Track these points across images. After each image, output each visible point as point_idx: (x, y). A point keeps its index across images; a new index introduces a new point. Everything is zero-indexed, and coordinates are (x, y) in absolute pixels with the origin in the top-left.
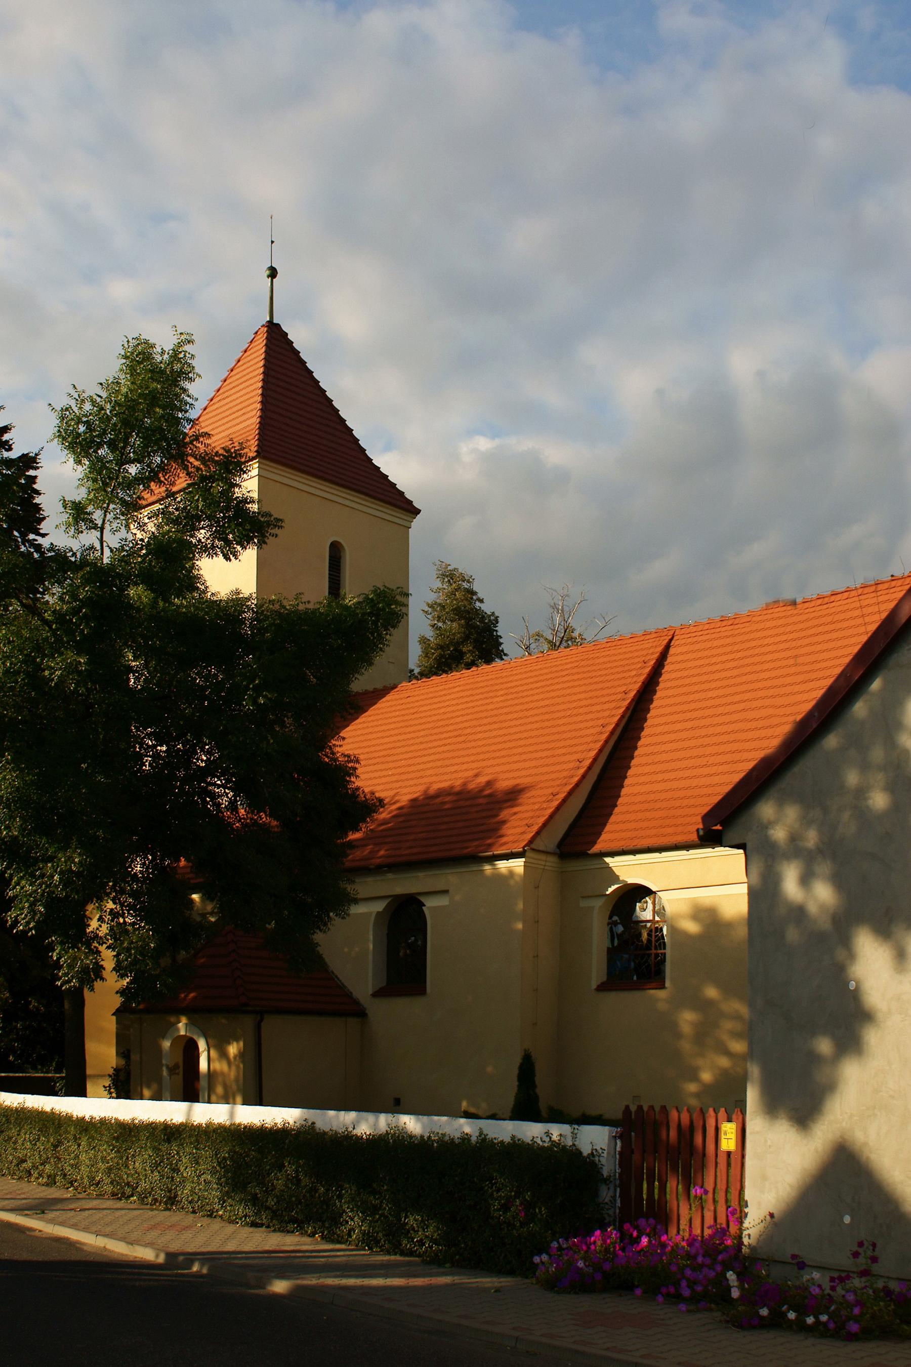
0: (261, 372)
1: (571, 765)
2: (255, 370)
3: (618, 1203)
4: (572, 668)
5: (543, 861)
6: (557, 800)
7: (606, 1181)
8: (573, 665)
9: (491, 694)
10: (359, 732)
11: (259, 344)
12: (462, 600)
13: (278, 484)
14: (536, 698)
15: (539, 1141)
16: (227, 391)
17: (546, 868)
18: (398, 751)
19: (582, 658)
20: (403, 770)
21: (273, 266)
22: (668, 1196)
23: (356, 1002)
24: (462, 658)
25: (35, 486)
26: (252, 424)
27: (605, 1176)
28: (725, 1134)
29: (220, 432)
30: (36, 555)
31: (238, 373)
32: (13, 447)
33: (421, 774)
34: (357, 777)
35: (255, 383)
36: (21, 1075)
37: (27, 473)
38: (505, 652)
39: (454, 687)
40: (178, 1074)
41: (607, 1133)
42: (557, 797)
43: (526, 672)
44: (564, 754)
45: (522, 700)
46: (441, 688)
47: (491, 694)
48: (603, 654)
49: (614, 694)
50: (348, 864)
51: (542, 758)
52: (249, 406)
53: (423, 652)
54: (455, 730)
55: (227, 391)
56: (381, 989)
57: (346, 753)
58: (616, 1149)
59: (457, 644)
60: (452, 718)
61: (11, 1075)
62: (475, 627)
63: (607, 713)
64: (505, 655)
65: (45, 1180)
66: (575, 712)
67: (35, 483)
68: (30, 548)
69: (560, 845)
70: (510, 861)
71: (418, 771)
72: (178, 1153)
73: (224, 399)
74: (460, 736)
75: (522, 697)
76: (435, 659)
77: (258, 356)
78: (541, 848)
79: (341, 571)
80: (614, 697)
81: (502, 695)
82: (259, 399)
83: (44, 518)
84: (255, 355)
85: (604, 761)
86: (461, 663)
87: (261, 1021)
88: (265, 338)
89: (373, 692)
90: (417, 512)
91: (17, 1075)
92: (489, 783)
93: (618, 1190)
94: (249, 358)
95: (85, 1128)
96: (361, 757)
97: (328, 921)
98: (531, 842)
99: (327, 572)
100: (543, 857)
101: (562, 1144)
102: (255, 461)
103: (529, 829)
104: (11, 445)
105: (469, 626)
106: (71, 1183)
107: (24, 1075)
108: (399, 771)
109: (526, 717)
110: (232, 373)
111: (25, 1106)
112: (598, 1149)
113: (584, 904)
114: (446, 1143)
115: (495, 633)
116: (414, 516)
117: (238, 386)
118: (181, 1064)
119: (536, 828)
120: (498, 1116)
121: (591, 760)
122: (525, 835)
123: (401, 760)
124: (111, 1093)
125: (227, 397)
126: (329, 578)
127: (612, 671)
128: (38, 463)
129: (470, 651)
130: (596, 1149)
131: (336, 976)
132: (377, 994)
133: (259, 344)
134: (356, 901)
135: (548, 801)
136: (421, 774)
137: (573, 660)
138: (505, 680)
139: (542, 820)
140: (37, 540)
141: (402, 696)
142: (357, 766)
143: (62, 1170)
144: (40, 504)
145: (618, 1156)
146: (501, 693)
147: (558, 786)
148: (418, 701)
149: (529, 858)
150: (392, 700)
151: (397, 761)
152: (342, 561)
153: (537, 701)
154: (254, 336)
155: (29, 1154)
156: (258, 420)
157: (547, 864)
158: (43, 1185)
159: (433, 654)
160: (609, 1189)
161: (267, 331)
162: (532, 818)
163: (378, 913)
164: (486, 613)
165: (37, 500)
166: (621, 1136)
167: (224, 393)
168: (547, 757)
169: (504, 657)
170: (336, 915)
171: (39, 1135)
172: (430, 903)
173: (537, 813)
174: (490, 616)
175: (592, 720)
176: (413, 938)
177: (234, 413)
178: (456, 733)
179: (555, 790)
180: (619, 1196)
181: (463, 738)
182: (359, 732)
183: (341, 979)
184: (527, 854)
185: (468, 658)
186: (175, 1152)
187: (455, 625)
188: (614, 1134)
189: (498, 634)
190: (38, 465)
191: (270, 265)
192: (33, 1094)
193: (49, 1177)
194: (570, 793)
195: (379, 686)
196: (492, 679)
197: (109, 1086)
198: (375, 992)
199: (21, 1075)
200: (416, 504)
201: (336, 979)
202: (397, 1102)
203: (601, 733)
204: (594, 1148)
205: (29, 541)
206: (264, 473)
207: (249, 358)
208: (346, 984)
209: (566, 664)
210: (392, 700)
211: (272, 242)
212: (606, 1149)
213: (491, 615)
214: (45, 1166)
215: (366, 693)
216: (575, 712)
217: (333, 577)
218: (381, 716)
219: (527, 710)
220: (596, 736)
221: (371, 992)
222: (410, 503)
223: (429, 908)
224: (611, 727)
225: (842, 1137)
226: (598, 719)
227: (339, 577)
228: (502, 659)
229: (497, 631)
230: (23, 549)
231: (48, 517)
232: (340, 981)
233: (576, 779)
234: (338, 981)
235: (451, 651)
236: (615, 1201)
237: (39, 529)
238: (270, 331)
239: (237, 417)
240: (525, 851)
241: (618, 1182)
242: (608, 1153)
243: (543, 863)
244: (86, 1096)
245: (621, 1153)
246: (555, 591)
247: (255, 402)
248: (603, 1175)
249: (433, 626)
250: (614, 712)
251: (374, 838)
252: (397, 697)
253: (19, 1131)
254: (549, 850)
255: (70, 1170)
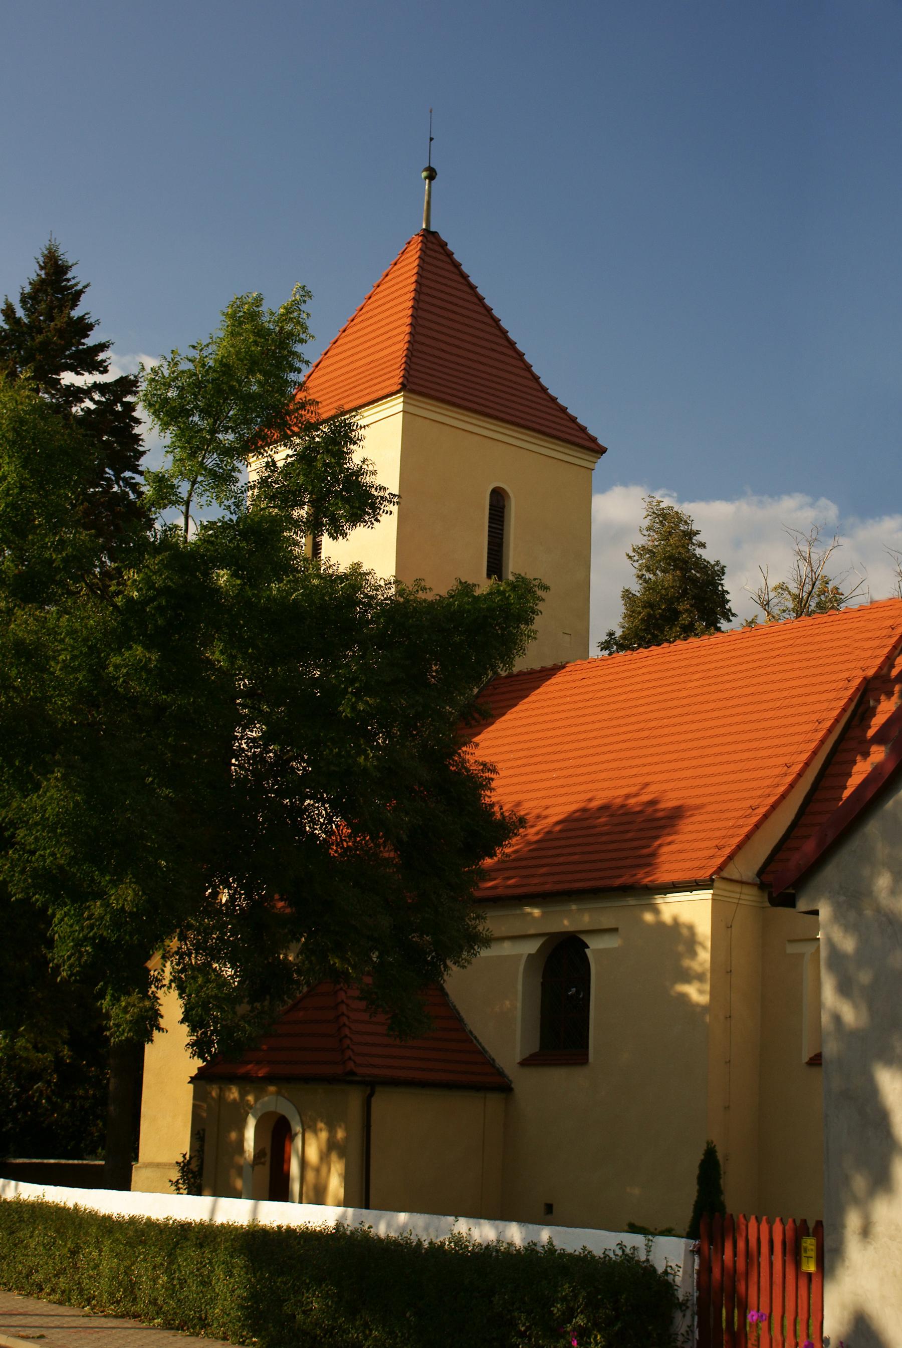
0: (412, 289)
1: (777, 771)
2: (405, 286)
3: (697, 1336)
4: (786, 647)
5: (737, 893)
6: (756, 815)
7: (683, 1306)
8: (786, 643)
9: (683, 678)
10: (519, 723)
11: (412, 256)
12: (678, 547)
13: (428, 421)
14: (740, 683)
15: (612, 1255)
16: (371, 310)
17: (741, 902)
18: (566, 747)
19: (797, 634)
20: (571, 772)
21: (432, 166)
22: (748, 1329)
23: (500, 1073)
24: (677, 619)
25: (134, 414)
26: (398, 350)
27: (680, 1301)
28: (806, 1251)
29: (360, 359)
30: (132, 496)
31: (385, 289)
32: (108, 368)
33: (593, 777)
34: (491, 790)
35: (404, 302)
36: (76, 1162)
37: (124, 400)
38: (733, 612)
39: (640, 668)
40: (264, 1164)
41: (683, 1247)
42: (757, 811)
43: (728, 651)
44: (770, 757)
45: (721, 687)
46: (624, 668)
47: (683, 678)
48: (824, 630)
49: (834, 681)
50: (477, 894)
51: (741, 761)
52: (395, 328)
53: (627, 610)
54: (638, 722)
55: (371, 310)
56: (531, 1056)
57: (481, 760)
58: (693, 1267)
59: (670, 601)
60: (635, 706)
61: (63, 1161)
62: (694, 580)
63: (825, 705)
64: (733, 615)
65: (58, 1296)
66: (786, 702)
67: (134, 410)
68: (126, 487)
69: (761, 873)
70: (694, 893)
71: (589, 773)
72: (210, 1263)
73: (367, 319)
74: (643, 730)
75: (722, 683)
76: (641, 619)
77: (410, 270)
78: (736, 876)
79: (505, 523)
80: (834, 686)
81: (697, 680)
82: (409, 321)
83: (144, 452)
84: (407, 268)
85: (820, 766)
86: (676, 626)
87: (371, 1095)
88: (418, 249)
89: (540, 671)
90: (603, 451)
91: (71, 1162)
92: (653, 802)
93: (696, 1318)
94: (398, 273)
95: (108, 1228)
96: (499, 766)
97: (445, 970)
98: (721, 868)
99: (487, 524)
100: (737, 888)
101: (636, 1258)
102: (399, 395)
103: (720, 853)
104: (107, 366)
105: (686, 580)
106: (88, 1300)
107: (80, 1162)
108: (565, 773)
109: (726, 708)
110: (379, 289)
111: (44, 1200)
112: (674, 1266)
113: (791, 949)
114: (512, 1255)
115: (720, 588)
116: (599, 456)
117: (384, 304)
118: (268, 1151)
119: (727, 851)
120: (674, 1232)
121: (802, 765)
122: (714, 860)
123: (569, 759)
124: (178, 1189)
125: (371, 317)
126: (489, 531)
127: (833, 652)
128: (138, 387)
129: (686, 610)
130: (671, 1267)
131: (475, 1038)
132: (526, 1063)
133: (412, 256)
134: (487, 942)
135: (745, 817)
136: (593, 777)
137: (786, 637)
138: (702, 660)
139: (736, 841)
140: (134, 478)
141: (574, 677)
142: (492, 776)
143: (79, 1283)
144: (140, 435)
145: (695, 1276)
146: (697, 676)
147: (760, 797)
148: (594, 684)
149: (719, 889)
150: (562, 683)
151: (564, 760)
152: (506, 510)
153: (741, 687)
154: (406, 246)
155: (41, 1262)
156: (406, 346)
157: (743, 897)
158: (55, 1303)
159: (640, 613)
160: (684, 1316)
161: (421, 241)
162: (724, 837)
163: (530, 955)
164: (708, 562)
165: (137, 430)
166: (698, 1251)
167: (367, 312)
168: (748, 759)
169: (731, 618)
170: (455, 963)
171: (54, 1238)
172: (595, 945)
173: (731, 832)
174: (713, 566)
175: (806, 713)
176: (574, 990)
177: (378, 336)
178: (637, 727)
179: (755, 802)
180: (697, 1327)
181: (646, 733)
182: (519, 723)
183: (481, 1040)
184: (716, 884)
185: (684, 619)
186: (207, 1261)
187: (669, 577)
188: (691, 1248)
189: (725, 588)
190: (138, 389)
191: (428, 165)
192: (56, 1185)
193: (63, 1292)
194: (774, 807)
195: (549, 664)
196: (687, 659)
197: (177, 1182)
198: (524, 1060)
199: (76, 1162)
200: (601, 442)
201: (475, 1041)
202: (549, 1208)
203: (817, 731)
204: (669, 1264)
205: (125, 480)
206: (411, 409)
207: (398, 273)
208: (487, 1048)
209: (778, 641)
210: (562, 683)
211: (431, 139)
212: (682, 1266)
213: (715, 565)
214: (59, 1278)
215: (532, 672)
216: (786, 702)
217: (493, 530)
218: (548, 703)
219: (727, 699)
220: (809, 734)
221: (518, 1060)
222: (594, 440)
223: (594, 951)
224: (828, 724)
225: (865, 1249)
226: (814, 712)
227: (502, 530)
228: (730, 621)
229: (722, 585)
230: (116, 489)
231: (149, 450)
232: (480, 1044)
233: (782, 789)
234: (477, 1044)
235: (664, 610)
236: (693, 1332)
237: (138, 465)
238: (425, 241)
239: (382, 342)
240: (712, 880)
241: (696, 1308)
242: (685, 1272)
243: (738, 896)
244: (129, 1190)
245: (699, 1273)
246: (802, 533)
247: (403, 324)
248: (678, 1299)
249: (640, 577)
250: (834, 704)
251: (507, 866)
252: (568, 678)
253: (32, 1232)
254: (744, 879)
255: (87, 1284)
